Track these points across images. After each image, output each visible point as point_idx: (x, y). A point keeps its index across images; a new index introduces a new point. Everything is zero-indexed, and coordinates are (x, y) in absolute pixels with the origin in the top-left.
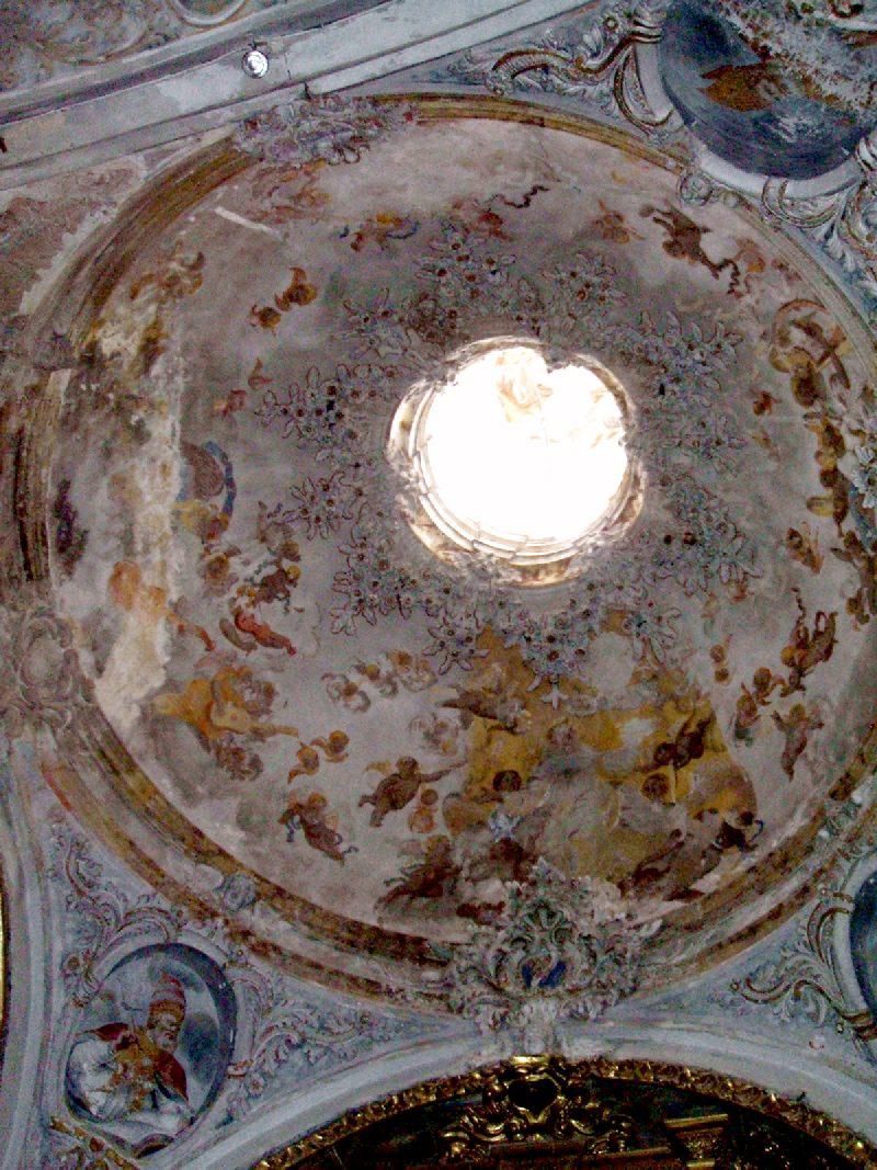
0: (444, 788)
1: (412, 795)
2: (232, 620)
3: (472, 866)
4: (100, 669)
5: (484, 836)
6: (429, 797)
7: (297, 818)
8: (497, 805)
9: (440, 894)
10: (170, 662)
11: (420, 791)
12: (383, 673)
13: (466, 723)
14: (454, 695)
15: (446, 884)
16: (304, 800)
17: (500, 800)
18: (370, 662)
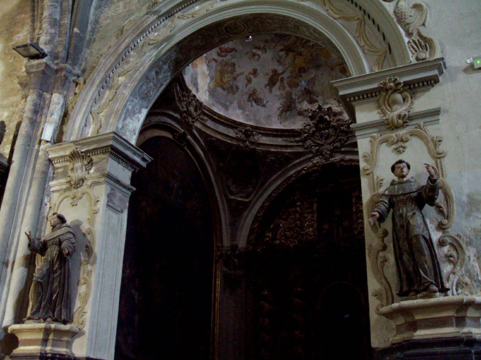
0: (285, 76)
1: (278, 80)
2: (219, 51)
3: (298, 98)
4: (197, 90)
5: (299, 88)
6: (282, 80)
7: (251, 98)
8: (301, 78)
9: (292, 110)
10: (210, 73)
11: (279, 78)
12: (262, 46)
13: (287, 54)
14: (282, 47)
15: (293, 105)
16: (251, 92)
17: (301, 76)
18: (257, 45)
